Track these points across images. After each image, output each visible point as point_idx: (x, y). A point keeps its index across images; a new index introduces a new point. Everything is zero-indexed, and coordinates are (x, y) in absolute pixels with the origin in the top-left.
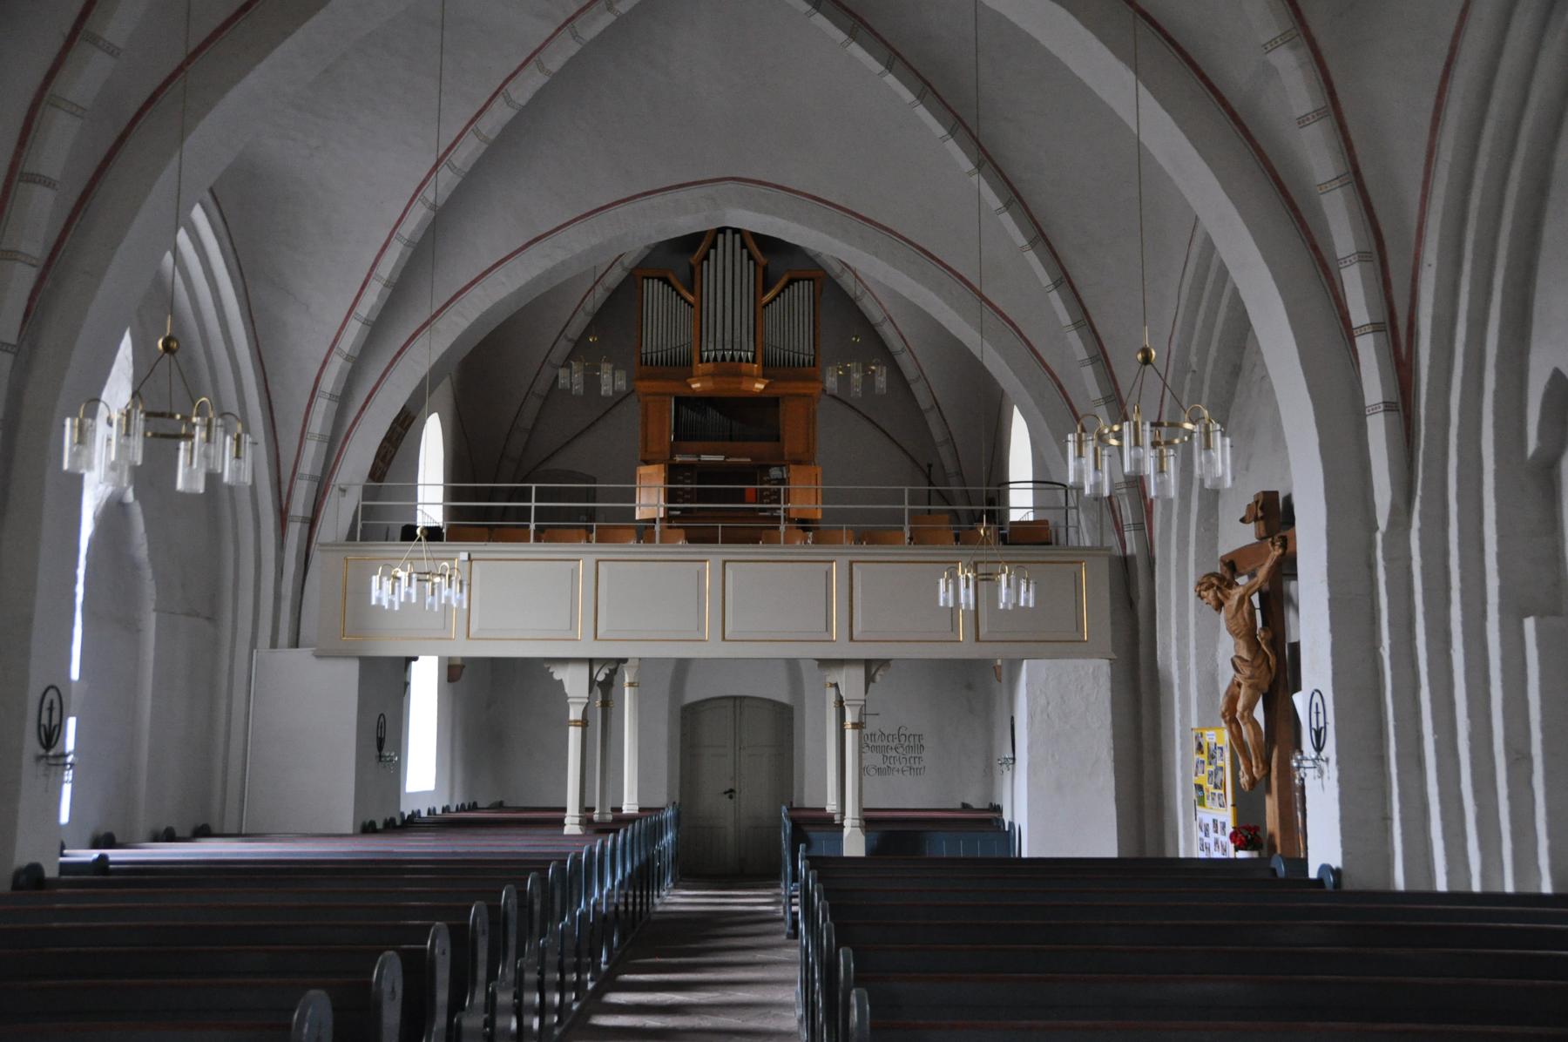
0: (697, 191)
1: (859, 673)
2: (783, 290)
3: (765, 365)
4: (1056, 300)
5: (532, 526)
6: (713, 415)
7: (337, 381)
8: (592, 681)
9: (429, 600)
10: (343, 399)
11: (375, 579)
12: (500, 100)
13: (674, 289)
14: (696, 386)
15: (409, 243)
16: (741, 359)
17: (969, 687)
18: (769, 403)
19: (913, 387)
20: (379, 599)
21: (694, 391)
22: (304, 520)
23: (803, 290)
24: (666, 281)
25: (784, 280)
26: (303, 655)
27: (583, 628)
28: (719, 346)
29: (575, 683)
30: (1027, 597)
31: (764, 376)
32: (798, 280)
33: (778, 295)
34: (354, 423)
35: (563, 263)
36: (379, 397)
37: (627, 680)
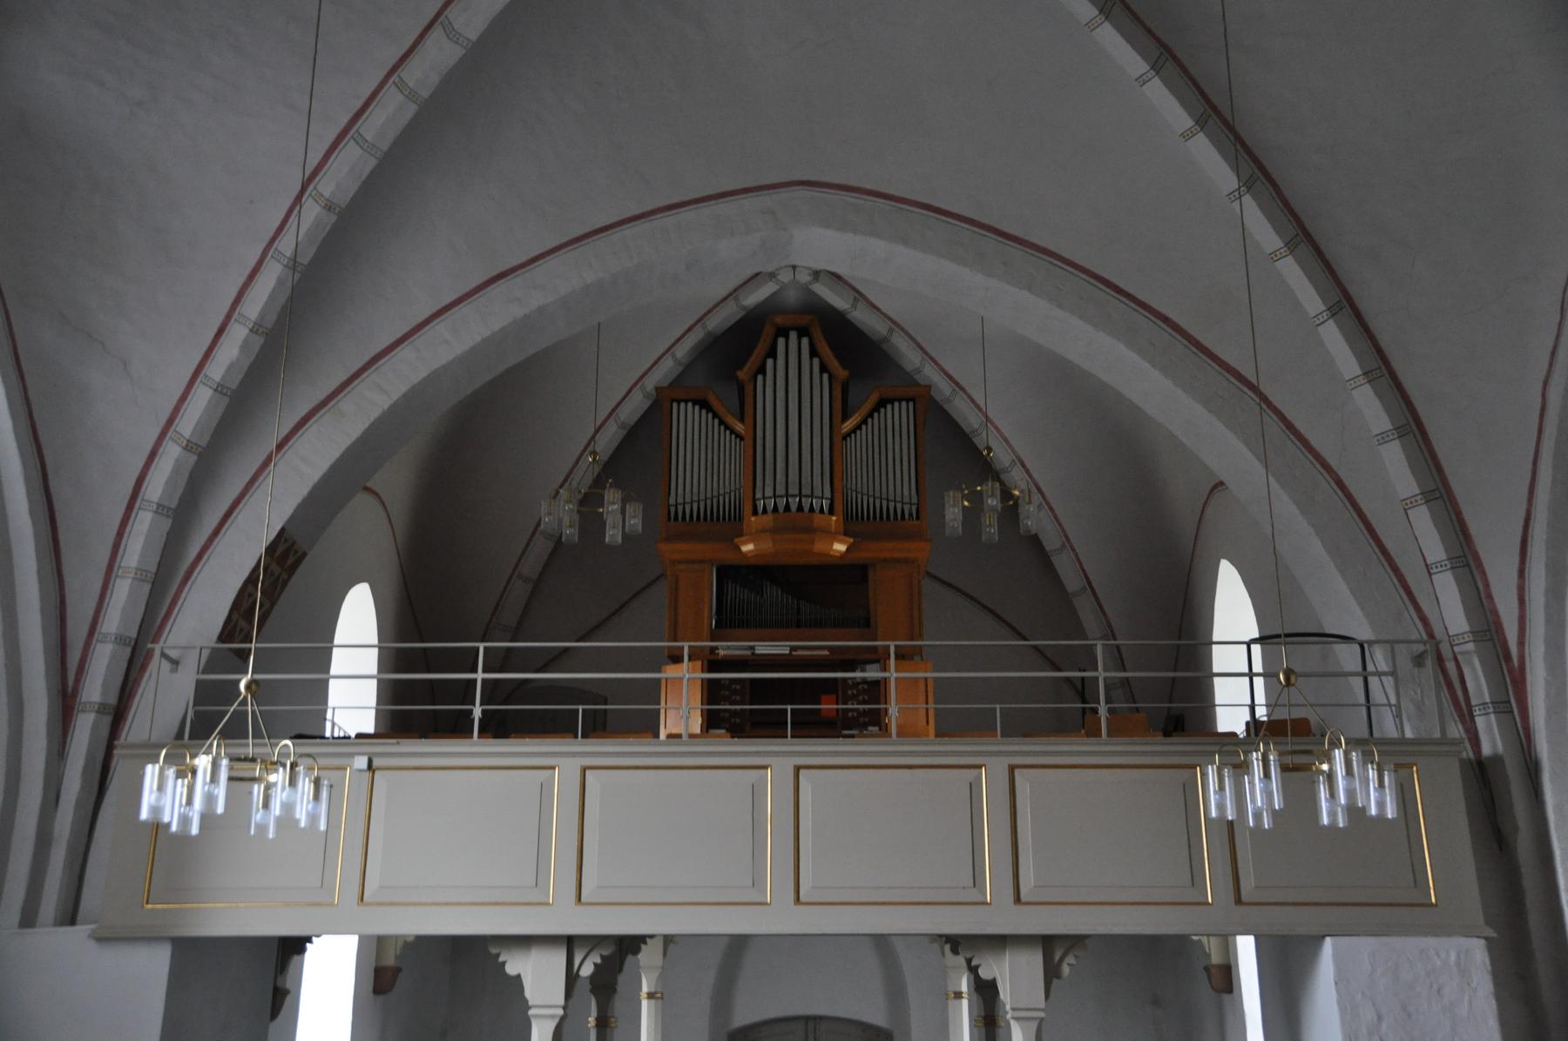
0: (748, 202)
1: (1032, 962)
2: (870, 415)
3: (848, 518)
4: (1332, 336)
5: (477, 712)
6: (772, 593)
7: (171, 482)
8: (571, 978)
9: (258, 816)
10: (182, 513)
11: (151, 772)
12: (437, 33)
13: (715, 415)
14: (748, 548)
15: (293, 264)
16: (812, 509)
17: (1156, 1002)
18: (853, 574)
19: (1056, 560)
20: (156, 810)
21: (744, 555)
22: (102, 709)
23: (899, 416)
24: (704, 404)
25: (873, 399)
26: (80, 932)
27: (557, 883)
28: (781, 490)
29: (541, 981)
30: (1378, 799)
31: (846, 534)
32: (892, 401)
33: (865, 422)
34: (199, 557)
35: (541, 310)
36: (242, 517)
37: (645, 989)
